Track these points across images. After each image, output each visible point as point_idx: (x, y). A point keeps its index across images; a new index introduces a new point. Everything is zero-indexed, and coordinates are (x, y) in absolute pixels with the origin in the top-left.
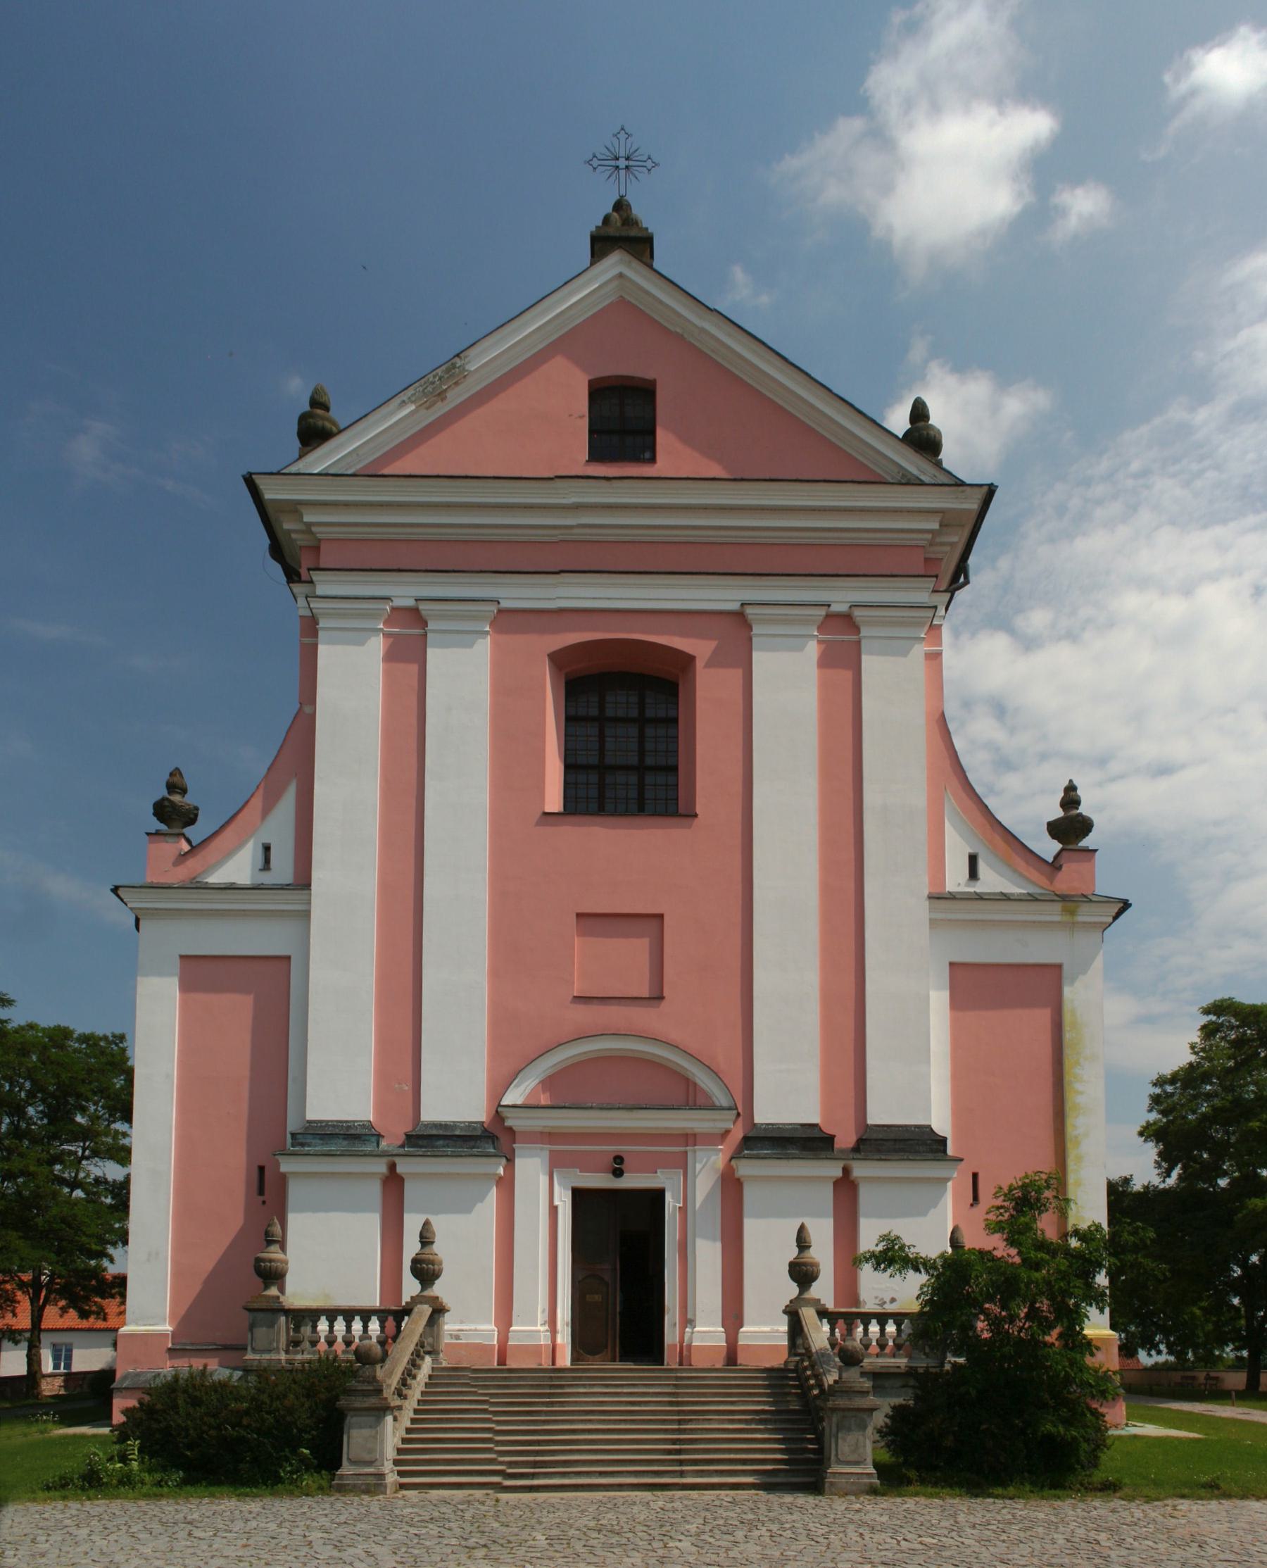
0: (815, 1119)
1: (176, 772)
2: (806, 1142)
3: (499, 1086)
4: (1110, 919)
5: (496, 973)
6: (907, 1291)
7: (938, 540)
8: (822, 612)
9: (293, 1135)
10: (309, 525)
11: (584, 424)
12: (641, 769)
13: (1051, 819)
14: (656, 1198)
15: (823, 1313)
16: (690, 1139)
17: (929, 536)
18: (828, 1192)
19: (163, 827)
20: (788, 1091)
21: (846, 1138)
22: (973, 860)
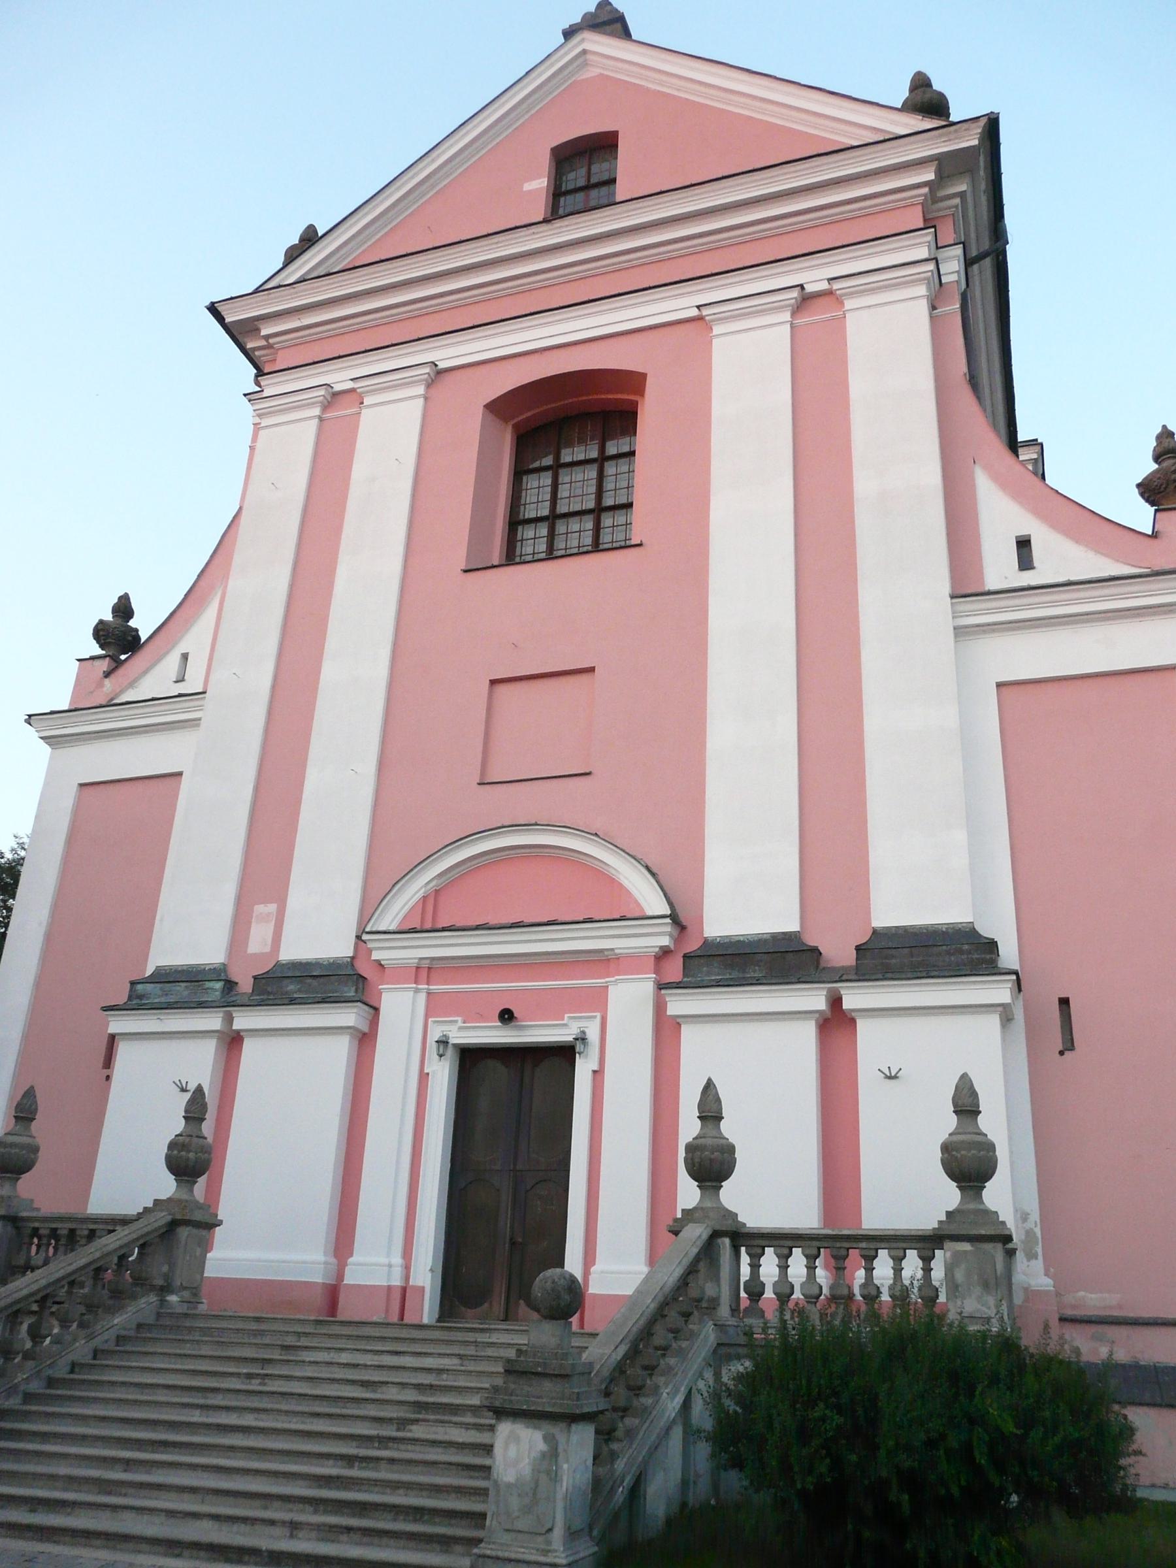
7: (941, 193)
8: (795, 294)
10: (267, 337)
12: (599, 510)
13: (1140, 481)
16: (604, 962)
17: (926, 190)
18: (808, 1032)
20: (748, 897)
21: (839, 950)
22: (1024, 544)
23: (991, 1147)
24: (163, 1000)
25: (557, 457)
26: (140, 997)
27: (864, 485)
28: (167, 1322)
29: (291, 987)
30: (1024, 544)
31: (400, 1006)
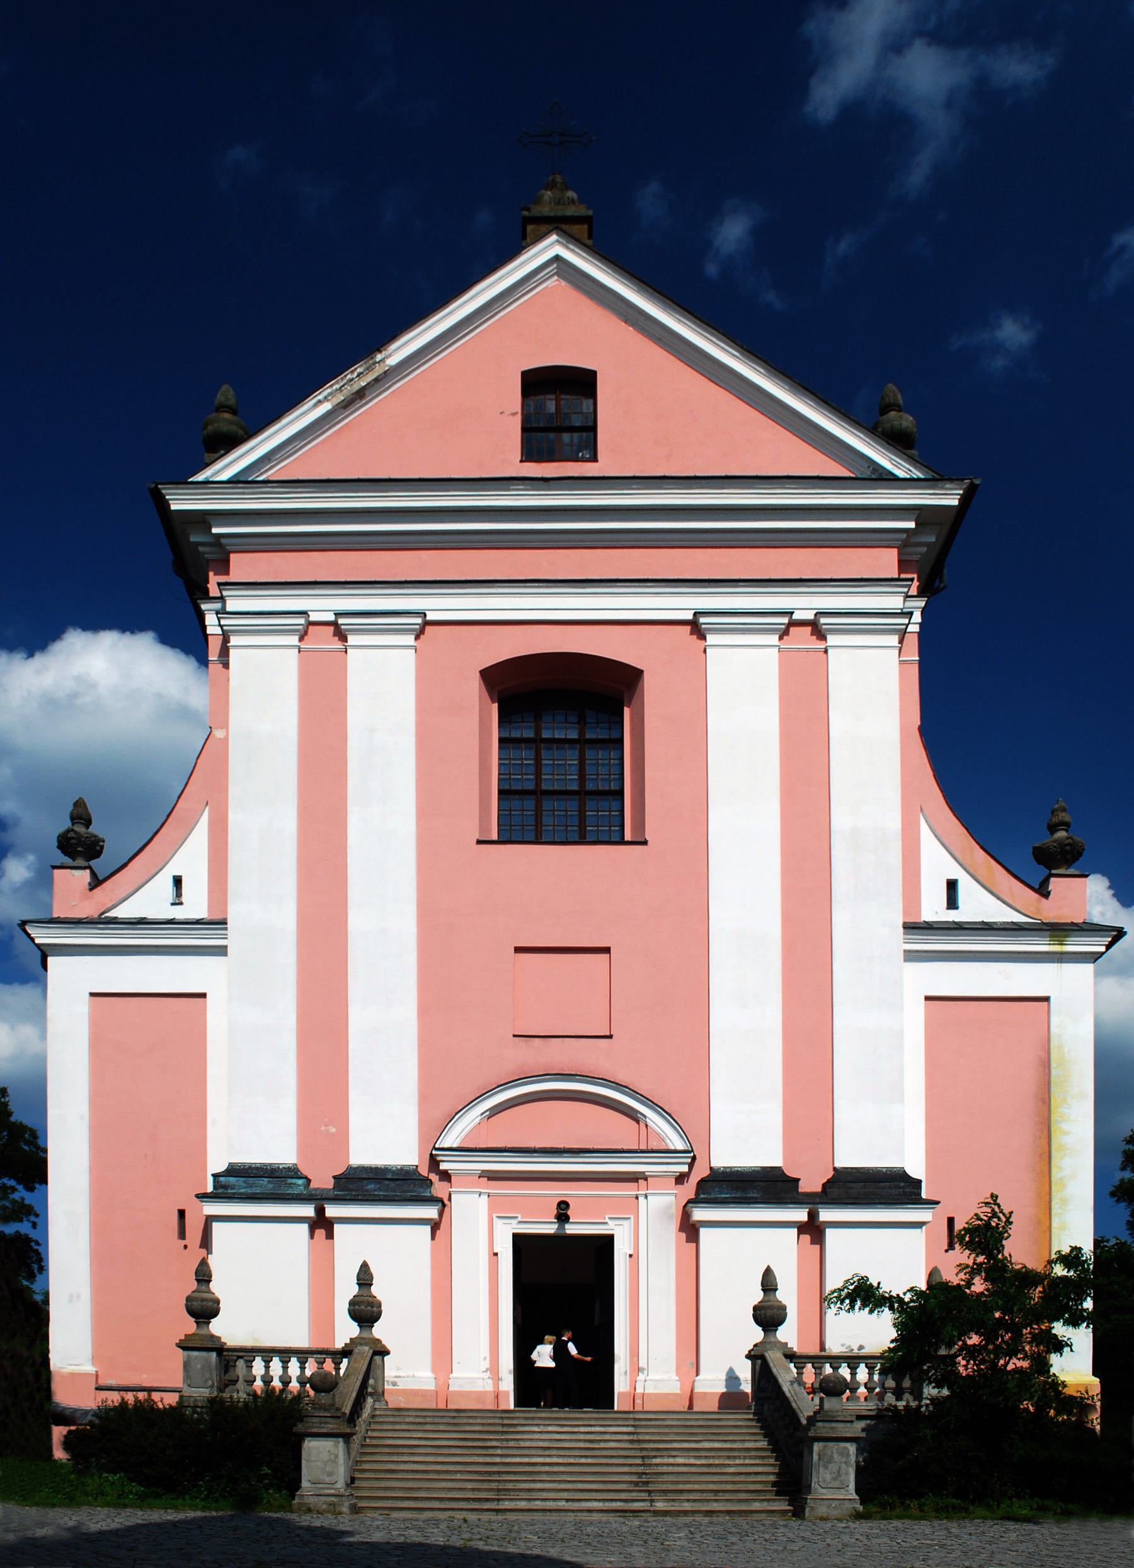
0: (777, 1162)
1: (79, 804)
2: (765, 1187)
3: (434, 1124)
4: (1103, 949)
5: (424, 1010)
6: (876, 1332)
9: (215, 1176)
11: (517, 423)
12: (582, 794)
14: (607, 1242)
15: (791, 1356)
17: (904, 536)
19: (67, 861)
20: (746, 1137)
21: (323, 1180)
22: (952, 885)
23: (784, 1308)
24: (249, 1191)
25: (538, 732)
26: (225, 1187)
27: (841, 820)
28: (377, 1419)
29: (371, 1186)
30: (952, 885)
31: (470, 1208)
